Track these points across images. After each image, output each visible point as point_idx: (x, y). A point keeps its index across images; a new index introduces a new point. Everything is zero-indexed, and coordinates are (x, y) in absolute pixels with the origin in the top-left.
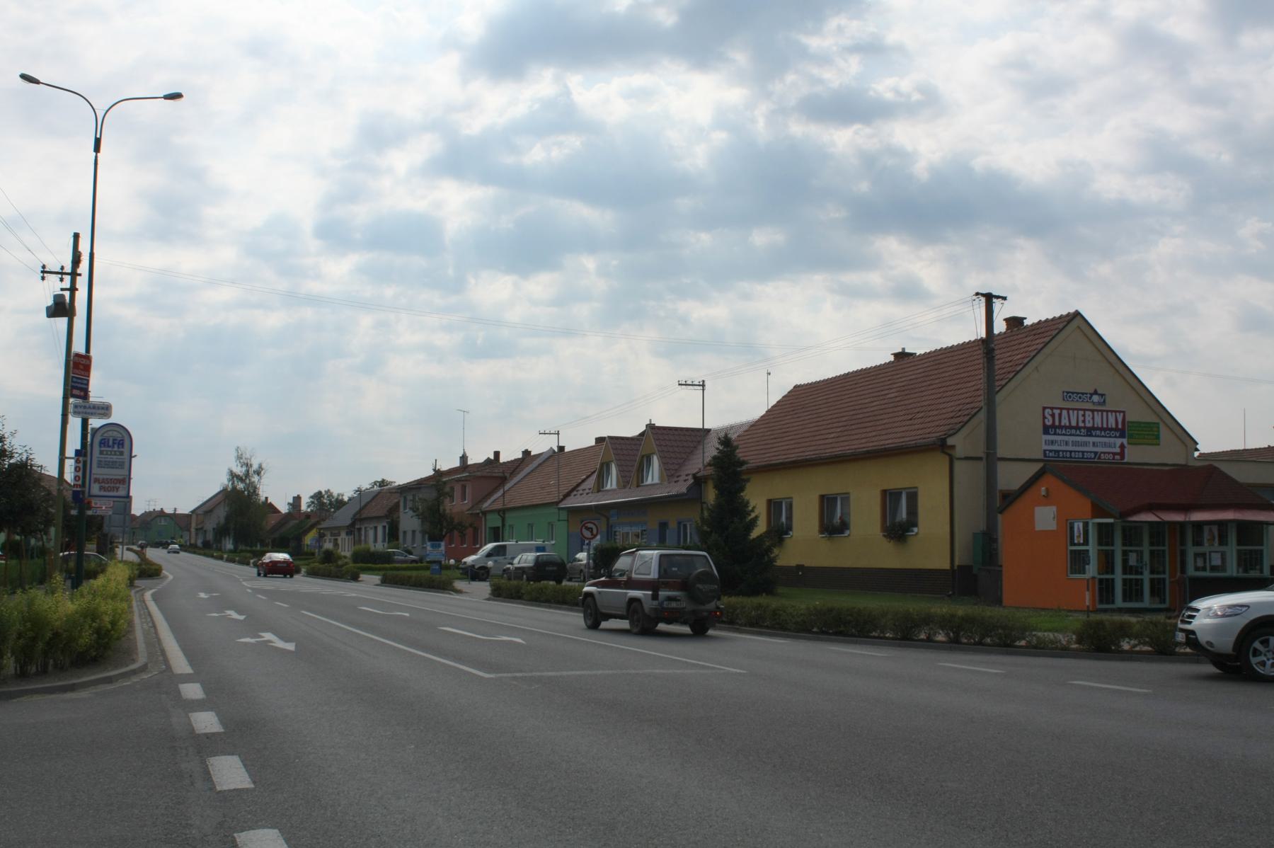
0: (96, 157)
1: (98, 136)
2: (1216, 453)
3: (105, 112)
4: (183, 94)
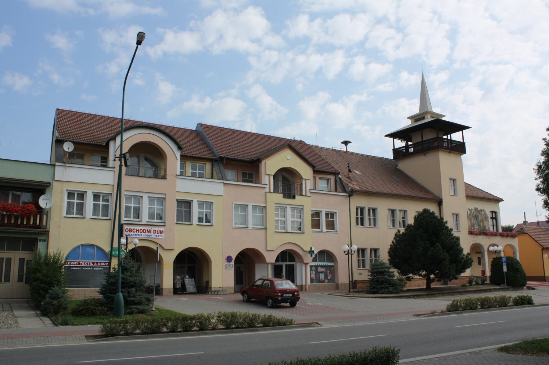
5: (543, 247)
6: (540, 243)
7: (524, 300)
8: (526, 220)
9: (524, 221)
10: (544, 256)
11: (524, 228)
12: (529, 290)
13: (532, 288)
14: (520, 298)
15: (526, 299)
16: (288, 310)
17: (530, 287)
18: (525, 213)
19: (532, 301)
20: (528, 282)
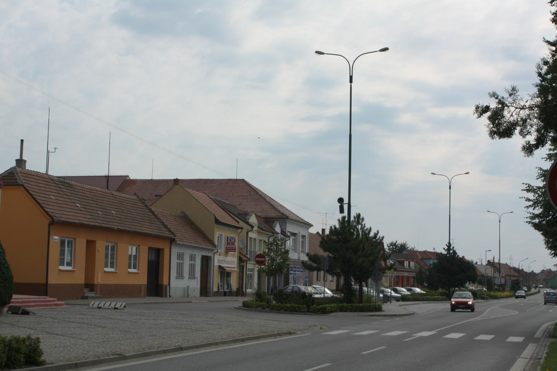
0: (351, 85)
1: (351, 75)
2: (162, 180)
3: (353, 62)
4: (389, 48)
5: (53, 219)
6: (47, 210)
7: (18, 351)
8: (24, 158)
9: (19, 158)
10: (51, 240)
11: (17, 173)
12: (16, 315)
13: (23, 310)
14: (5, 346)
15: (24, 349)
16: (147, 258)
17: (19, 308)
18: (22, 141)
19: (40, 354)
20: (14, 296)
